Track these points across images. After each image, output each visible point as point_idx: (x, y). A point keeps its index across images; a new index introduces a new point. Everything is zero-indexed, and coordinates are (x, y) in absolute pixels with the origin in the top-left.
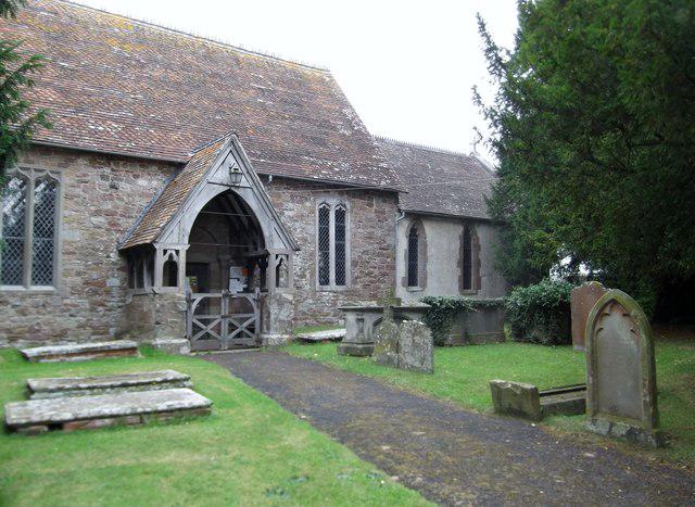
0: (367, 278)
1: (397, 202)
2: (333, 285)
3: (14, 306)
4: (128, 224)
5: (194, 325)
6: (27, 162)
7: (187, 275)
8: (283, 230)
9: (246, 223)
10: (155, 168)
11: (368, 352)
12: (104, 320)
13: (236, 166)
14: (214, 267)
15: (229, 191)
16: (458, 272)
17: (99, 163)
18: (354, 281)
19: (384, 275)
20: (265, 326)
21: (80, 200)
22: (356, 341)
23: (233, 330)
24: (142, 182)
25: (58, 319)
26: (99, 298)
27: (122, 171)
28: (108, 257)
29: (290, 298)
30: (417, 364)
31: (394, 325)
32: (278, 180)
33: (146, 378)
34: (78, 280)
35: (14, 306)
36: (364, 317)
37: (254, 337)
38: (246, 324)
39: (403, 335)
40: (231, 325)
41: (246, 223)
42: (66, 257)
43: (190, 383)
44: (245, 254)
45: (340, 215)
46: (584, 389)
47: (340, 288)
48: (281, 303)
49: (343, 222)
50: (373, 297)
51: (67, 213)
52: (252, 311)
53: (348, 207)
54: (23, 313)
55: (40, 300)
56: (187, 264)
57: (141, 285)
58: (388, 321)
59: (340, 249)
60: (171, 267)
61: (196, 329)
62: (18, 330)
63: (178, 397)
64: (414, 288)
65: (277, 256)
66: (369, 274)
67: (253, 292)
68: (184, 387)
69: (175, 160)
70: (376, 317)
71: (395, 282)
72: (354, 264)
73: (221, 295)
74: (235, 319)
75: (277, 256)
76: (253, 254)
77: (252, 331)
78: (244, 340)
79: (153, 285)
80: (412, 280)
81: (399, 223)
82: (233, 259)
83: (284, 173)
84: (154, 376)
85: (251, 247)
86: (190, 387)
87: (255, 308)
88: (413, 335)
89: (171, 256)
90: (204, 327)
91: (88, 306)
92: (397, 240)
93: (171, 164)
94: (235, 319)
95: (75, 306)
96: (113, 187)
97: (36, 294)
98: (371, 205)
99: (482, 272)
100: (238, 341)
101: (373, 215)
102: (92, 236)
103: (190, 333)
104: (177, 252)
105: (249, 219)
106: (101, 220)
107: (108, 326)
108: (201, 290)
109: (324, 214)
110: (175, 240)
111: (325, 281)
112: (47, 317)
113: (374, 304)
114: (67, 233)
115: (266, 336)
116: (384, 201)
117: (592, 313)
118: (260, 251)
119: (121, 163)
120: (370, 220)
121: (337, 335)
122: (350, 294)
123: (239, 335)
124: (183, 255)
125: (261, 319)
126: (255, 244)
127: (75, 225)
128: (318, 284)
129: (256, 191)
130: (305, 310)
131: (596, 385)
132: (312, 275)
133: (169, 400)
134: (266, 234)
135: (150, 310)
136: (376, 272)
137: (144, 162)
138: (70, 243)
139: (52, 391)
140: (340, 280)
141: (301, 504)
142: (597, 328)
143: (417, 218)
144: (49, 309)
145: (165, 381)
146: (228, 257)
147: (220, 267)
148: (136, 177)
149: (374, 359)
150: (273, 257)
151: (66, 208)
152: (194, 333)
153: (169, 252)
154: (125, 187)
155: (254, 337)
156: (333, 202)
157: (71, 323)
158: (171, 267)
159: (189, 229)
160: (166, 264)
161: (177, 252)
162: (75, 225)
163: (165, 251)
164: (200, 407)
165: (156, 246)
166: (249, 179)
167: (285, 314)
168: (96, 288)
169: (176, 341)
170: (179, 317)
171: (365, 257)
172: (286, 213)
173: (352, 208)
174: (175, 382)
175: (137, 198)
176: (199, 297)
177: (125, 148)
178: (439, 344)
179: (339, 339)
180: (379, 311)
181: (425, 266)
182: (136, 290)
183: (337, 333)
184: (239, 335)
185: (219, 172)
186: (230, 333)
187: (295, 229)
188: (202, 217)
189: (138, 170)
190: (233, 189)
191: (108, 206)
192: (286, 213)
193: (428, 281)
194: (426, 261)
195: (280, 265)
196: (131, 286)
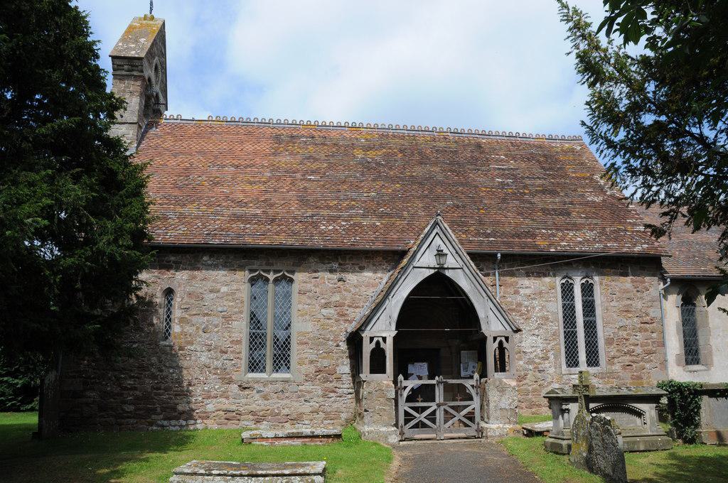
0: (628, 358)
2: (583, 366)
3: (258, 392)
5: (406, 413)
6: (268, 264)
12: (335, 406)
17: (328, 259)
19: (650, 353)
25: (295, 404)
26: (328, 385)
28: (338, 346)
34: (312, 369)
35: (258, 392)
38: (465, 412)
42: (301, 347)
45: (588, 290)
48: (502, 389)
51: (300, 307)
52: (471, 399)
54: (265, 398)
55: (279, 386)
59: (590, 327)
60: (378, 354)
61: (409, 418)
62: (261, 413)
65: (495, 339)
66: (629, 353)
69: (396, 248)
72: (609, 342)
74: (450, 407)
89: (378, 343)
91: (320, 392)
95: (309, 392)
97: (276, 381)
102: (323, 327)
103: (401, 421)
104: (384, 339)
106: (330, 311)
109: (567, 290)
110: (384, 329)
111: (572, 361)
112: (285, 402)
114: (302, 327)
119: (348, 257)
120: (626, 291)
124: (390, 341)
125: (482, 406)
127: (307, 317)
128: (564, 366)
132: (557, 357)
134: (481, 314)
136: (639, 350)
138: (304, 334)
140: (593, 360)
144: (287, 395)
150: (490, 341)
151: (300, 303)
152: (407, 421)
153: (375, 340)
155: (474, 427)
158: (378, 354)
160: (373, 352)
162: (307, 317)
168: (325, 374)
170: (386, 405)
171: (623, 334)
175: (363, 289)
177: (348, 242)
191: (336, 298)
192: (522, 291)
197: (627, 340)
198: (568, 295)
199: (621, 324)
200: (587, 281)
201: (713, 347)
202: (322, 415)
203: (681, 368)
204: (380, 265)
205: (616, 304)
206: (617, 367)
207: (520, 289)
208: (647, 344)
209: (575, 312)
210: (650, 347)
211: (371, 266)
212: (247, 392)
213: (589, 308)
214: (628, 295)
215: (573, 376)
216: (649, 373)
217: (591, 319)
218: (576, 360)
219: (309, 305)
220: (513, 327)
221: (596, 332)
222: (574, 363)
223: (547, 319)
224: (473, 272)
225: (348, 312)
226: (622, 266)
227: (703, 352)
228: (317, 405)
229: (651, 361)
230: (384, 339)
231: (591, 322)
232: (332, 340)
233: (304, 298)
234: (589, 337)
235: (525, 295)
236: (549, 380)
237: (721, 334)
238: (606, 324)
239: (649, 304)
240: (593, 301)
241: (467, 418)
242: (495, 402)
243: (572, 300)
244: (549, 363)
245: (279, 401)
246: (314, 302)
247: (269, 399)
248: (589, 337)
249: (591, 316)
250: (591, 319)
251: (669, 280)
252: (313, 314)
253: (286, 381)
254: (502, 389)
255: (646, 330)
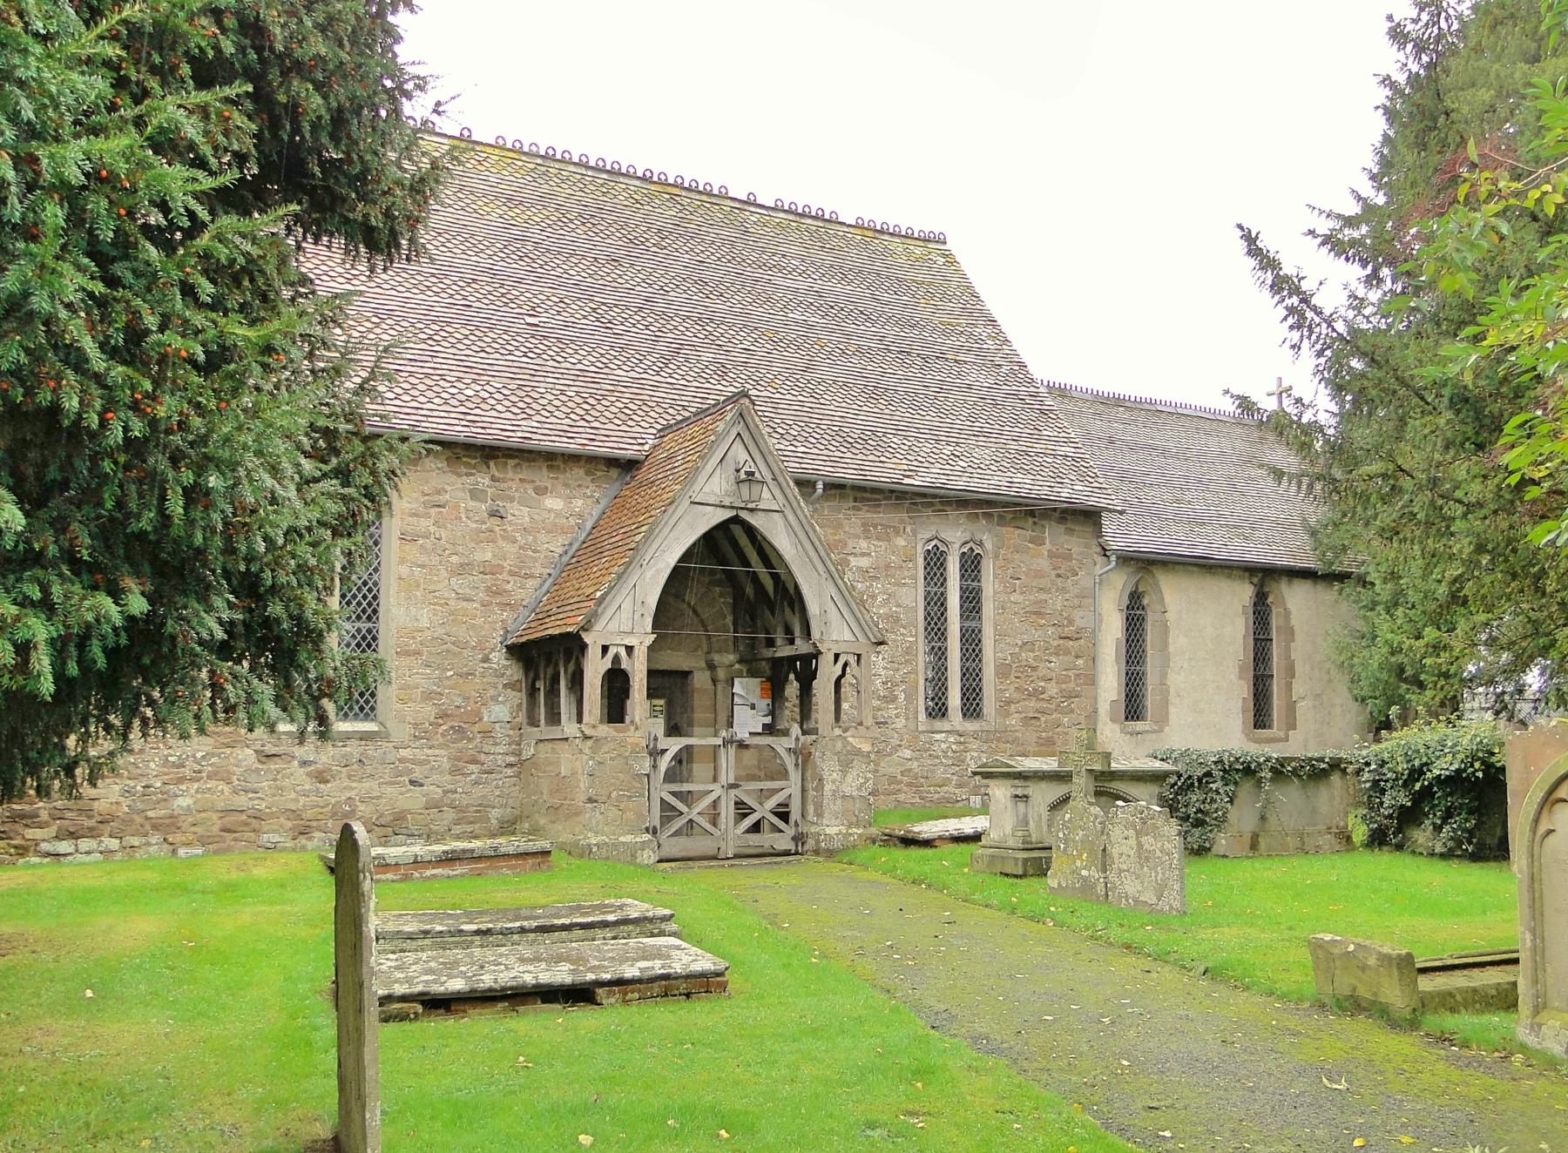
0: (1033, 703)
1: (1098, 526)
4: (526, 592)
5: (665, 805)
7: (650, 696)
8: (853, 602)
9: (769, 584)
10: (578, 472)
11: (1038, 867)
12: (479, 791)
13: (751, 467)
14: (701, 679)
15: (736, 520)
16: (1244, 690)
17: (467, 465)
18: (1005, 705)
19: (1070, 696)
20: (811, 809)
21: (428, 543)
22: (1011, 843)
23: (745, 815)
24: (553, 503)
25: (389, 790)
27: (514, 478)
29: (866, 748)
30: (1149, 897)
31: (1096, 810)
32: (836, 488)
33: (583, 915)
34: (429, 711)
35: (304, 763)
36: (1029, 791)
37: (790, 831)
38: (771, 803)
39: (1117, 833)
40: (739, 804)
41: (769, 584)
43: (673, 927)
44: (768, 653)
45: (971, 565)
46: (1516, 961)
47: (971, 726)
49: (977, 579)
50: (1046, 746)
52: (784, 775)
53: (988, 545)
56: (651, 673)
57: (554, 718)
58: (1085, 808)
59: (972, 642)
60: (616, 682)
63: (657, 954)
64: (1139, 726)
65: (837, 656)
66: (1036, 694)
67: (786, 733)
68: (662, 934)
70: (1054, 791)
71: (1095, 711)
72: (1003, 671)
73: (719, 741)
74: (748, 792)
75: (837, 656)
76: (784, 651)
77: (784, 817)
78: (766, 839)
79: (580, 721)
80: (1133, 707)
81: (1102, 580)
82: (740, 661)
83: (848, 474)
84: (602, 908)
85: (779, 636)
86: (674, 934)
87: (791, 767)
88: (1139, 834)
89: (617, 658)
90: (683, 808)
91: (446, 765)
92: (1098, 618)
93: (612, 462)
94: (748, 792)
95: (421, 763)
96: (494, 514)
98: (1039, 542)
99: (1298, 689)
100: (754, 839)
101: (1044, 564)
105: (776, 577)
107: (484, 807)
108: (673, 730)
109: (935, 562)
111: (938, 710)
113: (1050, 764)
115: (813, 829)
116: (1070, 531)
117: (1536, 795)
118: (801, 647)
119: (512, 462)
120: (1039, 574)
121: (968, 831)
122: (999, 737)
123: (756, 828)
124: (641, 654)
125: (804, 790)
126: (789, 631)
128: (922, 716)
129: (791, 517)
130: (895, 771)
131: (1539, 950)
133: (645, 958)
134: (813, 608)
135: (574, 773)
136: (1052, 689)
137: (553, 459)
139: (410, 937)
140: (972, 707)
141: (1562, 231)
142: (1542, 829)
143: (1144, 564)
145: (625, 922)
146: (732, 657)
147: (714, 681)
148: (541, 491)
149: (1052, 881)
151: (402, 561)
152: (665, 820)
154: (518, 513)
155: (790, 831)
156: (955, 534)
157: (412, 800)
158: (616, 682)
159: (653, 601)
161: (630, 649)
163: (605, 649)
164: (703, 975)
165: (588, 638)
166: (777, 492)
167: (854, 782)
169: (628, 838)
172: (854, 561)
173: (998, 548)
174: (643, 924)
175: (543, 537)
176: (674, 745)
178: (1200, 851)
179: (976, 838)
180: (1061, 777)
181: (1164, 675)
182: (545, 731)
183: (968, 826)
184: (756, 828)
185: (716, 479)
186: (737, 823)
187: (873, 597)
188: (678, 576)
189: (543, 476)
190: (744, 515)
191: (486, 554)
192: (854, 561)
193: (1172, 710)
194: (1165, 663)
195: (843, 674)
196: (533, 722)
197: (1034, 669)
198: (935, 574)
199: (1026, 638)
200: (972, 550)
201: (1172, 690)
202: (450, 815)
203: (1117, 727)
204: (580, 486)
205: (1021, 599)
206: (1013, 721)
207: (851, 558)
208: (1067, 679)
209: (946, 609)
210: (1072, 685)
211: (560, 488)
212: (274, 765)
213: (972, 602)
214: (1042, 583)
215: (937, 736)
216: (1066, 734)
217: (973, 624)
218: (943, 704)
219: (423, 566)
220: (871, 636)
221: (980, 651)
222: (940, 709)
223: (898, 620)
224: (804, 521)
225: (509, 587)
226: (1035, 523)
227: (1150, 701)
228: (439, 790)
229: (1072, 711)
230: (630, 649)
231: (973, 631)
232: (474, 648)
233: (412, 551)
234: (967, 660)
235: (859, 569)
236: (895, 742)
237: (1185, 666)
238: (1000, 636)
239: (1076, 601)
240: (980, 590)
241: (776, 814)
242: (833, 782)
243: (942, 585)
244: (896, 708)
245: (354, 785)
246: (435, 560)
247: (327, 781)
248: (967, 660)
249: (974, 618)
250: (973, 624)
251: (1113, 558)
252: (432, 588)
253: (365, 737)
254: (847, 760)
255: (1067, 652)
